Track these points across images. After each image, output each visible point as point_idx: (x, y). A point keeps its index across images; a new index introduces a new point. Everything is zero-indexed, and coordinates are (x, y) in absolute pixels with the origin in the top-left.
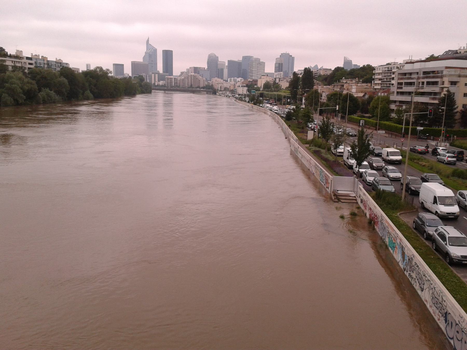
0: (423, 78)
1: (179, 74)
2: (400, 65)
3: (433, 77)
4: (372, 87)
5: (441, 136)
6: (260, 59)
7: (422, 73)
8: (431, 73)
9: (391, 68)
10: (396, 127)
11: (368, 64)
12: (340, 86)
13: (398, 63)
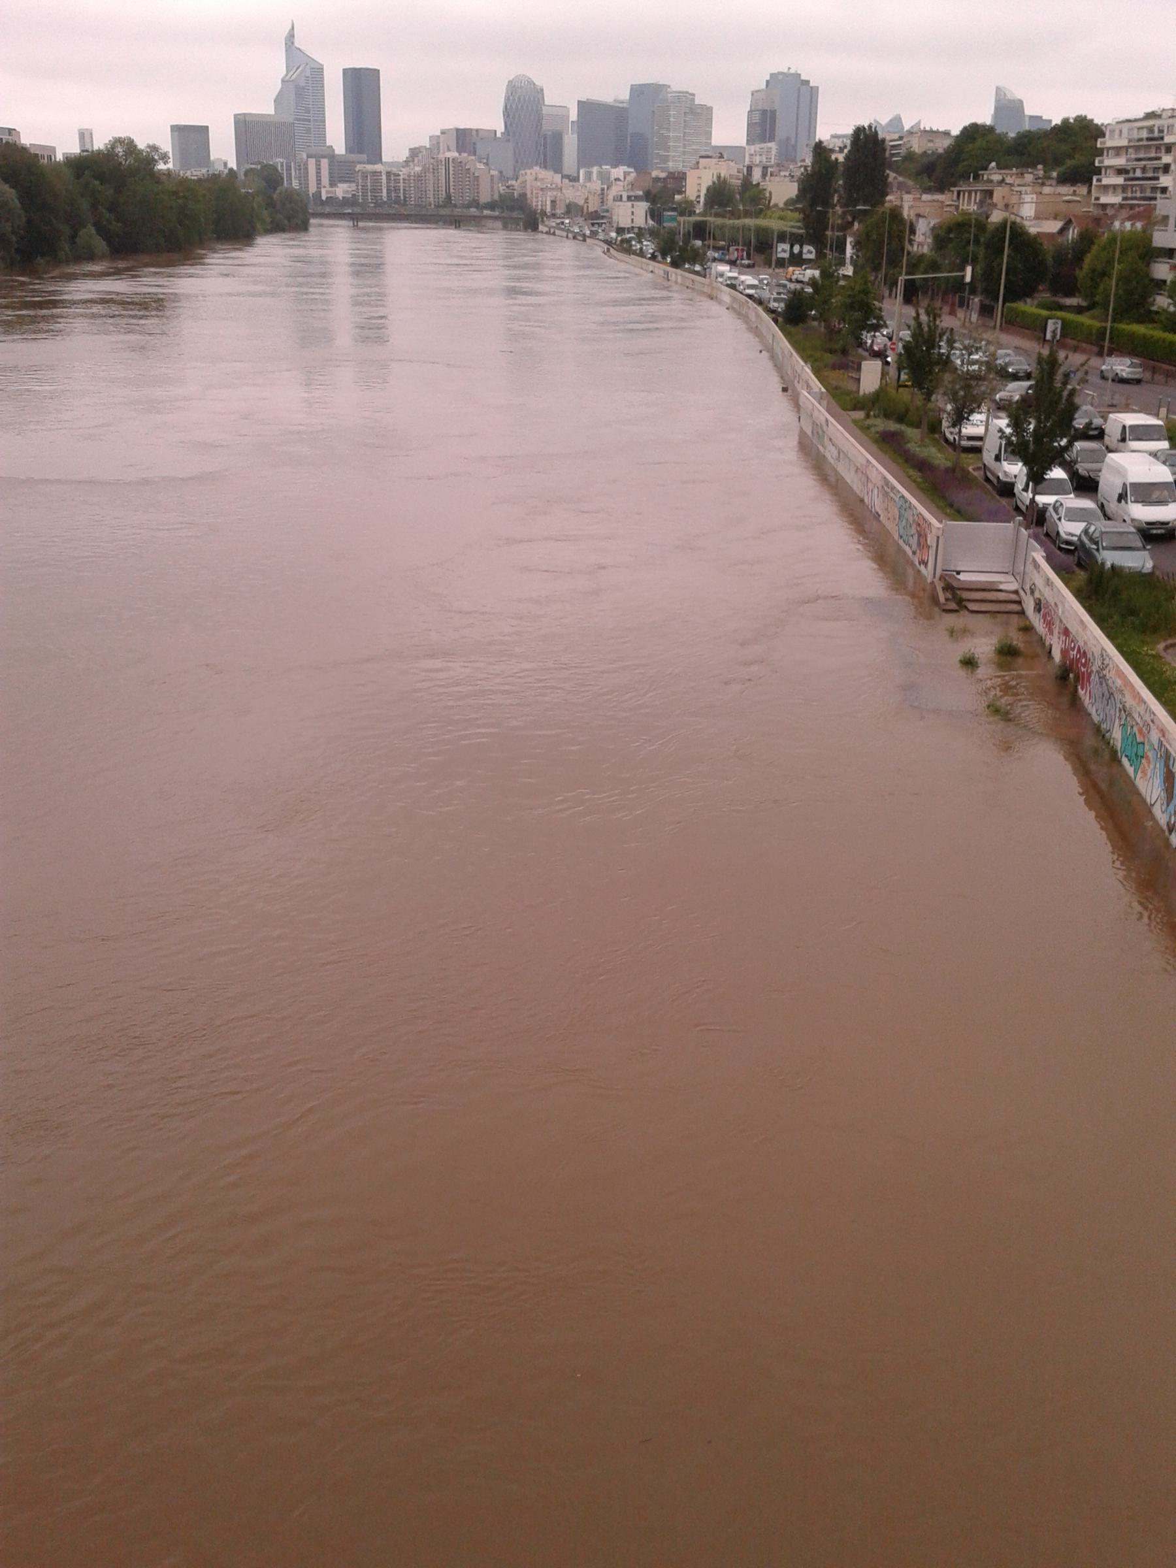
1: (404, 155)
6: (693, 95)
9: (1161, 131)
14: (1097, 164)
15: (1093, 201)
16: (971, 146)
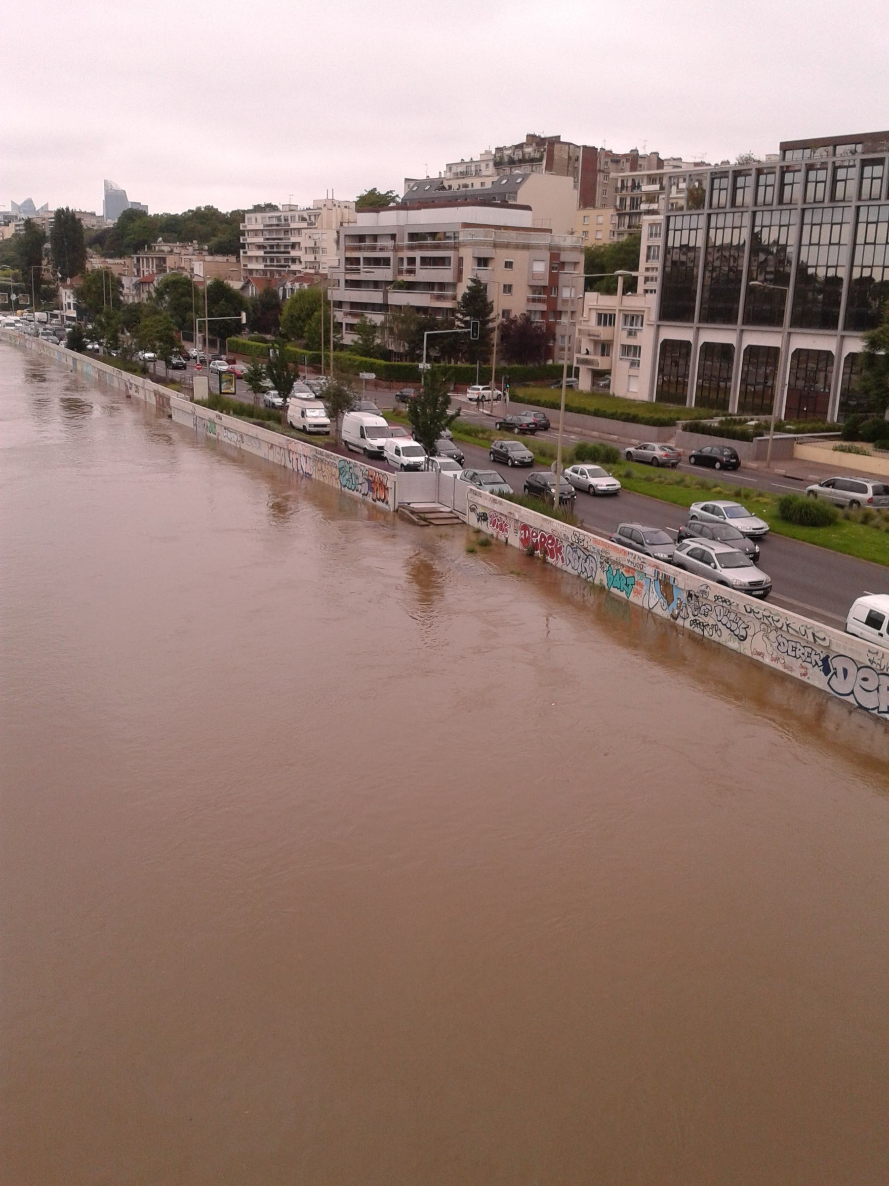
0: (411, 248)
2: (308, 211)
3: (437, 247)
4: (241, 266)
5: (491, 380)
7: (406, 237)
8: (429, 238)
9: (286, 220)
10: (371, 363)
11: (209, 206)
12: (154, 260)
13: (297, 206)
14: (241, 241)
15: (242, 267)
16: (132, 225)
